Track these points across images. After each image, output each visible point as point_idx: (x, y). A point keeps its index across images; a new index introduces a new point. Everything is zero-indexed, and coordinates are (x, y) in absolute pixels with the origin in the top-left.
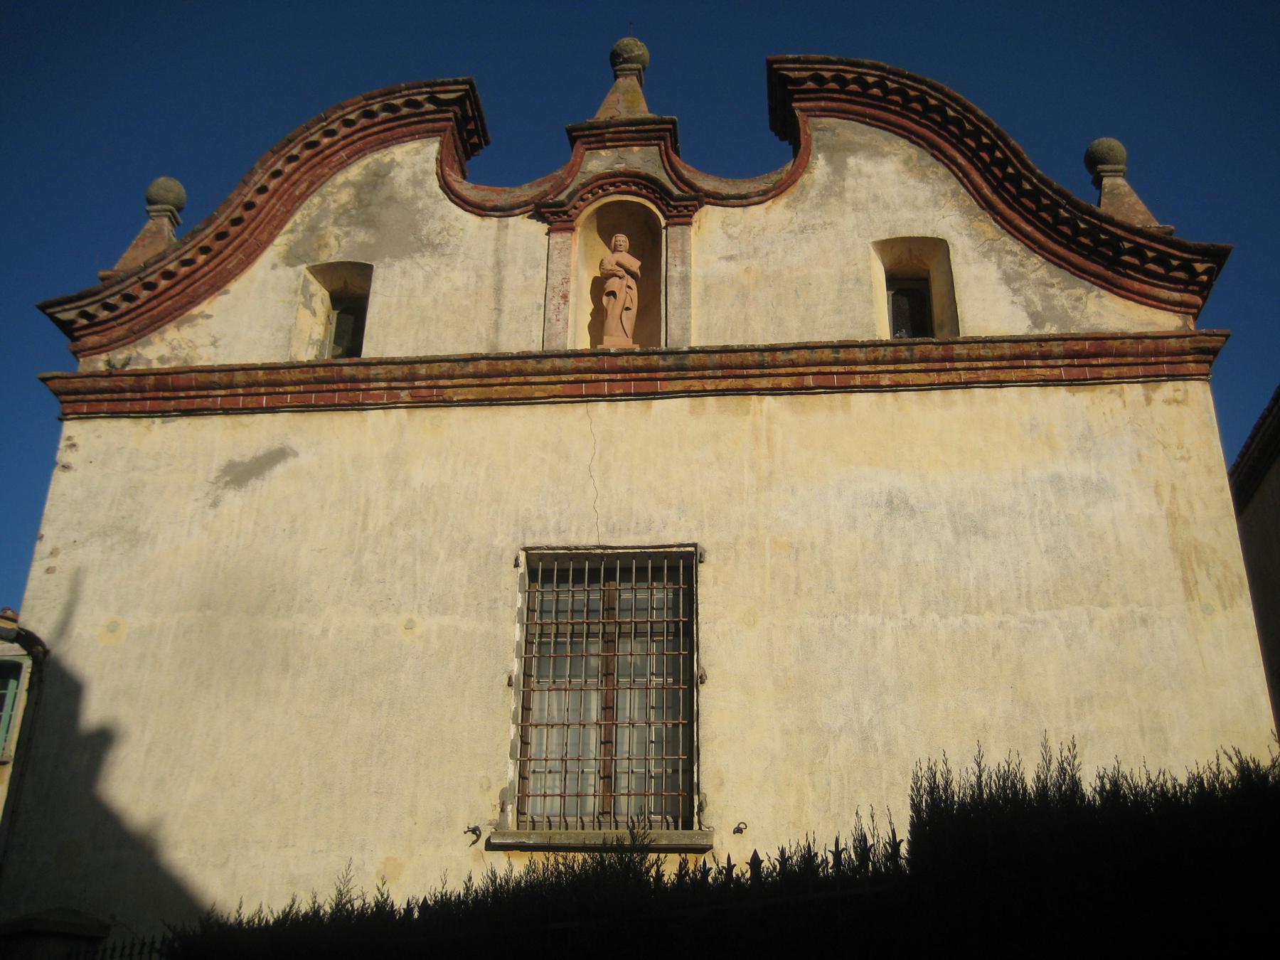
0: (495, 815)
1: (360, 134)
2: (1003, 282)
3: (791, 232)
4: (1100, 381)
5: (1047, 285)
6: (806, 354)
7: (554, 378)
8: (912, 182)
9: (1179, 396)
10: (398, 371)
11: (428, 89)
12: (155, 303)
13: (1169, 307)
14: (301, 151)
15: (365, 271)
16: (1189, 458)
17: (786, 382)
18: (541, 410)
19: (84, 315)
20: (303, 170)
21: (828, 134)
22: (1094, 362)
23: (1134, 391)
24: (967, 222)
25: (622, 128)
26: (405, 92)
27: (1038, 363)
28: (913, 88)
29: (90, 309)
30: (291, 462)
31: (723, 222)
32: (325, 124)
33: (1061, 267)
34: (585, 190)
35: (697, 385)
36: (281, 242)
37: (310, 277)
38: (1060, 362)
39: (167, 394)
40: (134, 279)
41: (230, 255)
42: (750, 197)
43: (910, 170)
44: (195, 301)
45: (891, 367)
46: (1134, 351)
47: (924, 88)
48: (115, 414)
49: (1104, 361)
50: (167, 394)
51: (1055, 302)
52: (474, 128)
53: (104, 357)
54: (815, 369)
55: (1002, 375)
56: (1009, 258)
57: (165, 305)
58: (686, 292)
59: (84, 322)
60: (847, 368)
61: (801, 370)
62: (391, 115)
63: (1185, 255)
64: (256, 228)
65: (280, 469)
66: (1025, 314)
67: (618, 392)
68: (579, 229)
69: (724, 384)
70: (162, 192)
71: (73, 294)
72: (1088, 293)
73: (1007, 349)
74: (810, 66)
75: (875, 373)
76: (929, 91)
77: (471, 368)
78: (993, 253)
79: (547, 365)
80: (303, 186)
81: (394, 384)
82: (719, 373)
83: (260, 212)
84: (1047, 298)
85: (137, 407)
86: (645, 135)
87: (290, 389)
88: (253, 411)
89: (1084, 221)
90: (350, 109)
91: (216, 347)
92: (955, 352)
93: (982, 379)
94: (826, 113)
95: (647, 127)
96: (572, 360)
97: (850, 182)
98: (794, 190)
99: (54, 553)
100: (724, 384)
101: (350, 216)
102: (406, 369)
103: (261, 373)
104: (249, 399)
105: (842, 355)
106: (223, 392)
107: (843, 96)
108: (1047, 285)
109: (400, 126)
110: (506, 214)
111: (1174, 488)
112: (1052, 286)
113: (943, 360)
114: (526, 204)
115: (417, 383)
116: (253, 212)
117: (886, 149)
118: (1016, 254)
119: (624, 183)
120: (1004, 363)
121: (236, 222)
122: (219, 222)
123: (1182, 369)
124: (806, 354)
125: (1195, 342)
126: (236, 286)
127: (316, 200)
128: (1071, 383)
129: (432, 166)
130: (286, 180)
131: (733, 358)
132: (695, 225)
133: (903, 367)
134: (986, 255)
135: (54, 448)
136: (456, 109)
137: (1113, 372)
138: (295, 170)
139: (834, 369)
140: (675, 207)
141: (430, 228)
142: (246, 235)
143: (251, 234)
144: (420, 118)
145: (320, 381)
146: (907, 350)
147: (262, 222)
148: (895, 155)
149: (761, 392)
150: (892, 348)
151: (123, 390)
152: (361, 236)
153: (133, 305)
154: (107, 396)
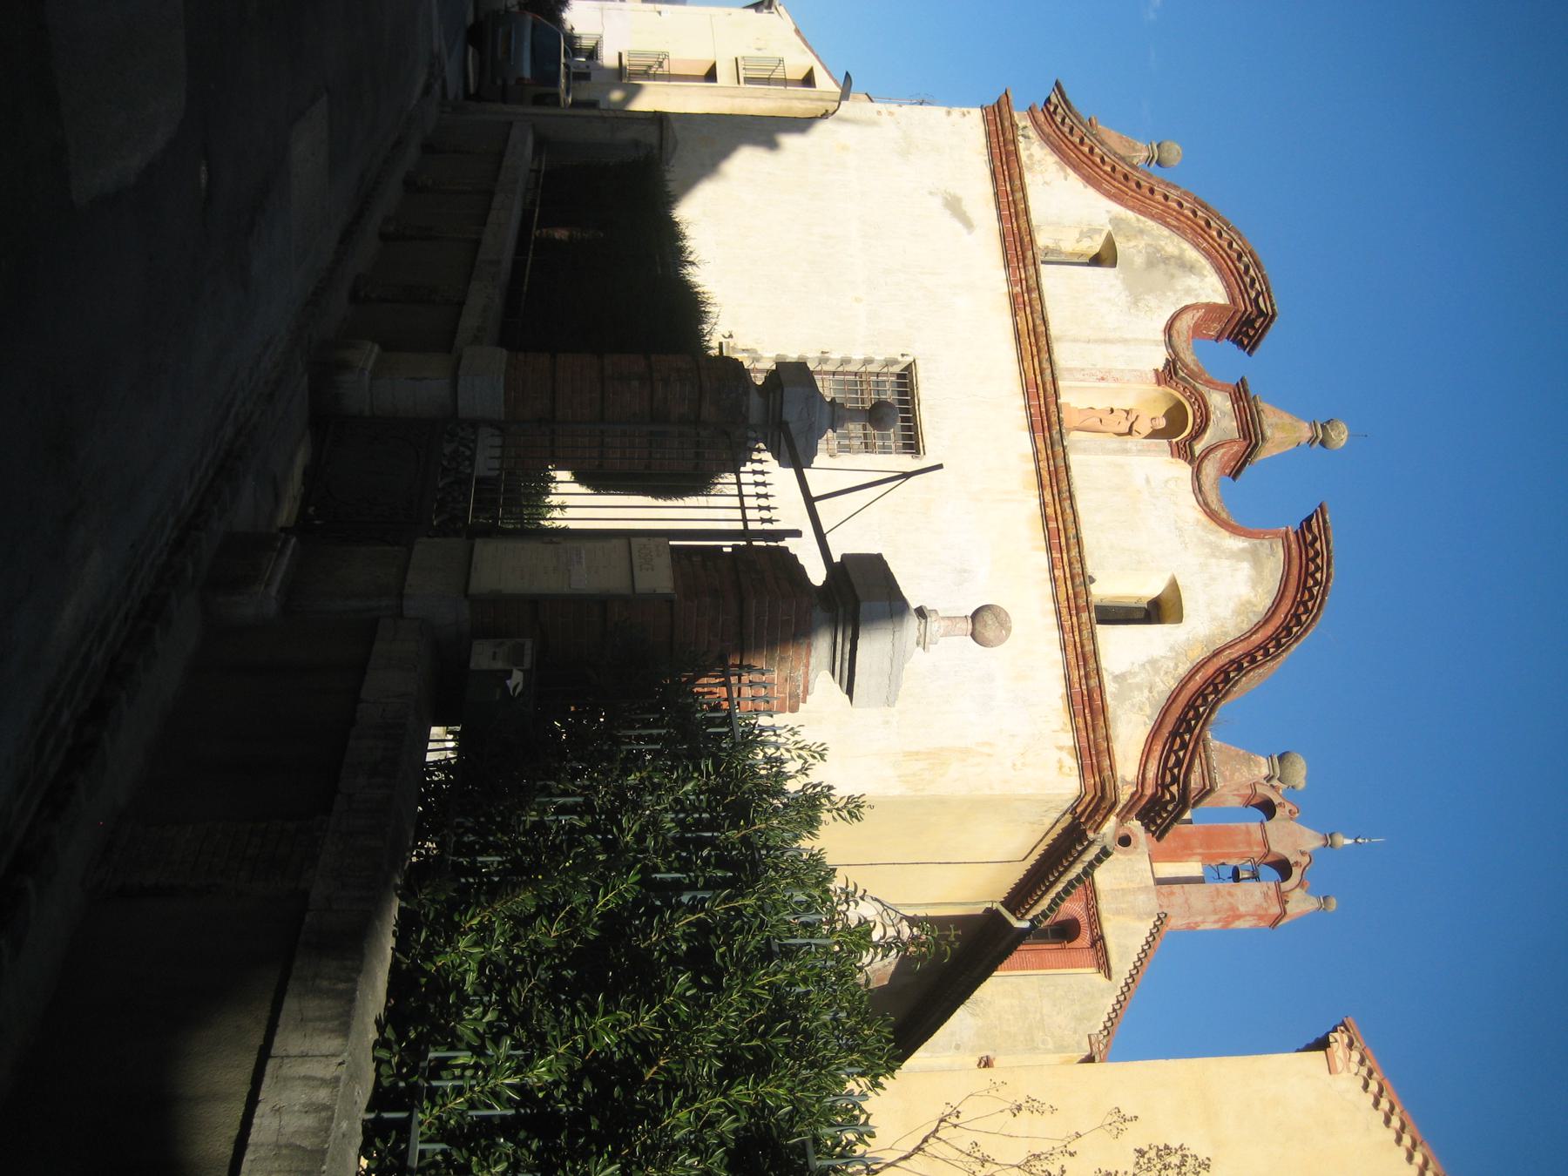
0: (740, 346)
1: (1224, 255)
2: (1150, 658)
3: (1176, 521)
4: (1073, 716)
5: (1151, 688)
6: (1070, 518)
7: (1038, 372)
8: (1232, 605)
9: (1066, 770)
10: (1032, 282)
11: (1264, 290)
12: (1072, 147)
13: (1141, 771)
14: (1201, 218)
15: (1114, 264)
16: (1015, 769)
17: (1050, 511)
18: (1015, 367)
19: (1056, 108)
20: (1189, 222)
21: (1268, 551)
22: (1086, 711)
23: (1068, 739)
24: (1200, 639)
25: (1248, 411)
26: (1260, 276)
27: (1082, 673)
28: (1313, 606)
29: (1060, 110)
30: (965, 231)
31: (1178, 478)
32: (1225, 228)
33: (1168, 700)
34: (1192, 389)
35: (1042, 456)
36: (1130, 215)
37: (1104, 235)
38: (1084, 687)
39: (1004, 159)
40: (1084, 130)
41: (1114, 186)
42: (1201, 495)
43: (1242, 605)
44: (1076, 168)
45: (1068, 575)
46: (1098, 736)
47: (1315, 611)
48: (988, 135)
49: (1089, 718)
50: (1004, 159)
51: (1136, 693)
52: (1251, 334)
53: (1029, 123)
54: (1061, 527)
55: (1070, 648)
56: (1172, 665)
57: (1072, 154)
58: (1115, 452)
59: (1052, 109)
60: (1064, 548)
61: (1060, 519)
62: (1242, 272)
63: (1182, 777)
64: (1137, 199)
65: (958, 226)
66: (1124, 670)
67: (1032, 410)
68: (1160, 388)
69: (1045, 474)
70: (1166, 148)
71: (1067, 97)
72: (1148, 717)
73: (1089, 648)
74: (1322, 532)
75: (1063, 566)
76: (1313, 614)
77: (1038, 322)
78: (1174, 654)
79: (1046, 365)
80: (1175, 223)
81: (1024, 282)
82: (1052, 468)
83: (1149, 199)
84: (1139, 687)
85: (994, 145)
86: (1246, 427)
87: (1015, 225)
88: (998, 208)
89: (1205, 710)
90: (1240, 243)
91: (1043, 185)
92: (1083, 614)
93: (1066, 636)
94: (1286, 550)
95: (1251, 426)
96: (1051, 379)
97: (1227, 563)
98: (1213, 526)
99: (891, 114)
100: (1045, 474)
101: (1155, 254)
102: (1035, 285)
103: (1023, 206)
104: (1006, 204)
105: (1073, 541)
106: (1009, 189)
107: (1304, 562)
108: (1151, 688)
109: (1236, 279)
110: (1168, 345)
111: (989, 755)
112: (1151, 692)
113: (1077, 608)
114: (1176, 354)
115: (1026, 295)
116: (1148, 194)
117: (1260, 590)
118: (1176, 670)
119: (1201, 414)
120: (1079, 650)
121: (1138, 185)
122: (1135, 173)
123: (1088, 774)
124: (1070, 518)
125: (1109, 780)
126: (1091, 192)
127: (1166, 232)
128: (1070, 697)
129: (1204, 300)
130: (1178, 213)
131: (1063, 475)
132: (1173, 460)
133: (1069, 583)
134: (1172, 648)
135: (961, 105)
136: (1255, 312)
137: (1081, 725)
138: (1187, 217)
139: (1063, 540)
140: (1185, 445)
141: (1152, 301)
142: (1130, 193)
143: (1131, 196)
144: (1244, 291)
145: (1021, 240)
146: (1081, 582)
147: (1143, 202)
148: (1256, 596)
149: (1042, 496)
150: (1081, 572)
151: (1003, 135)
152: (1139, 260)
153: (1067, 134)
154: (1000, 127)
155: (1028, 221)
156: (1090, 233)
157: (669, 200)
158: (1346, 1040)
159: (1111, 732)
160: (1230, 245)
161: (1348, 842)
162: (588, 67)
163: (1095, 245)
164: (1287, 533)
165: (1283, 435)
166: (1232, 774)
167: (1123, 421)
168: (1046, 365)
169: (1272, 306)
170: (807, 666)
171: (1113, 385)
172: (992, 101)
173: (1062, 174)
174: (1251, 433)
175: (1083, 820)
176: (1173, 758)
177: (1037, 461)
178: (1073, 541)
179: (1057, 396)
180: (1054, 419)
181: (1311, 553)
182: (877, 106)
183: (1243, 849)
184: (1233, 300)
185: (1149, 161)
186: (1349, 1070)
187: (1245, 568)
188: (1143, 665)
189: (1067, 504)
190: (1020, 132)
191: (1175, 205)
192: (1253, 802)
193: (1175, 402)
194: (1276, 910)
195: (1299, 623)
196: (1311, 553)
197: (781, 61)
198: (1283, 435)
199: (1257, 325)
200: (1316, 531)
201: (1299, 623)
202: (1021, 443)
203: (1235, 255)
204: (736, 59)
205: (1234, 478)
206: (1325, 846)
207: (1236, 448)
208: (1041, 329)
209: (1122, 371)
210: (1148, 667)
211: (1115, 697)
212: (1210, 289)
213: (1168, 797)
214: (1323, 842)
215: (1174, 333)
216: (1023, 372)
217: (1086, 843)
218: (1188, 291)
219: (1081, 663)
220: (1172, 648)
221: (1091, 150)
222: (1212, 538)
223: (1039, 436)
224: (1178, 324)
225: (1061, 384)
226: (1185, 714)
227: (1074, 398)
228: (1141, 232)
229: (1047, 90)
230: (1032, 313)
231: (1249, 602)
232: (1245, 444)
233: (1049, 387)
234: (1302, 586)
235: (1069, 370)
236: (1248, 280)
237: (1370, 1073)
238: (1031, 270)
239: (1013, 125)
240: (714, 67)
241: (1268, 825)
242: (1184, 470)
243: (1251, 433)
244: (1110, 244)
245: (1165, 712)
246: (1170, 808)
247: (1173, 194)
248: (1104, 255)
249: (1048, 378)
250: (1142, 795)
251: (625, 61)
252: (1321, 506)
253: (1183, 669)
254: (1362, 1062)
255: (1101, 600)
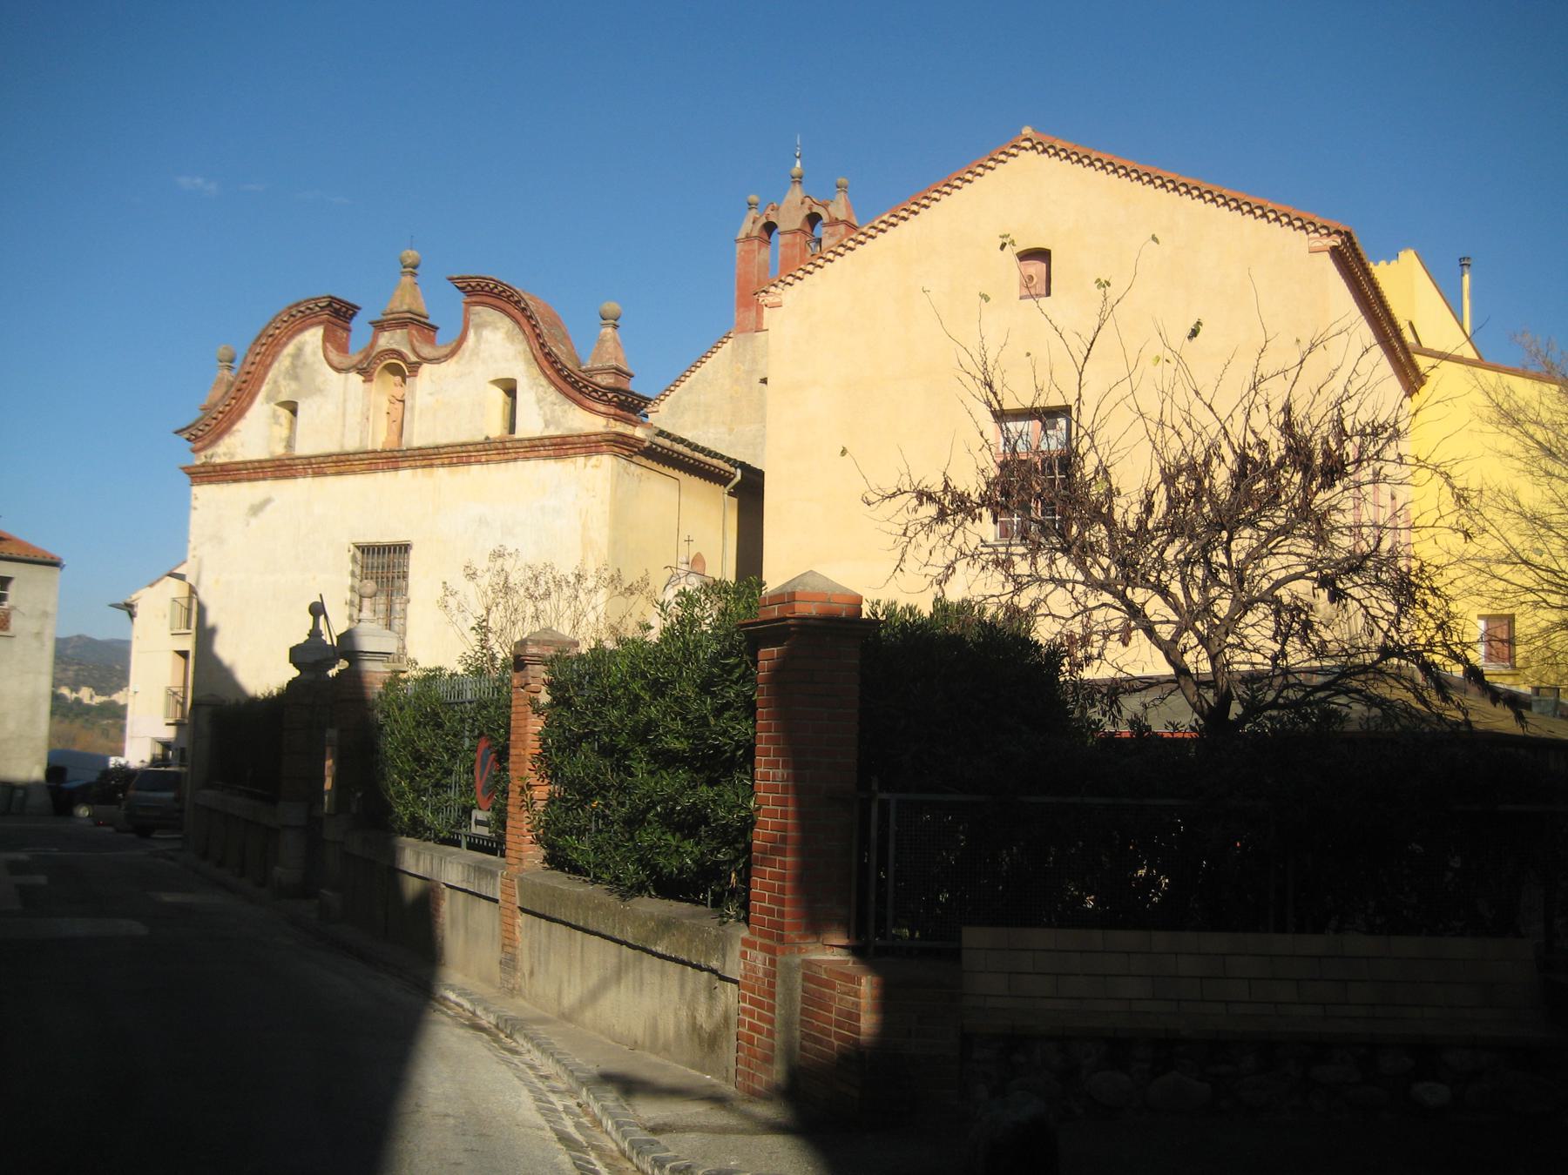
4: (567, 456)
7: (362, 462)
8: (508, 345)
9: (598, 463)
10: (305, 461)
15: (296, 403)
17: (446, 461)
21: (477, 316)
23: (581, 460)
27: (542, 448)
35: (413, 463)
36: (264, 389)
37: (277, 407)
38: (550, 448)
44: (233, 423)
45: (484, 453)
48: (210, 482)
49: (568, 446)
54: (456, 455)
55: (528, 455)
56: (541, 389)
59: (193, 437)
65: (269, 508)
68: (375, 380)
77: (330, 459)
79: (357, 457)
82: (421, 458)
84: (553, 411)
87: (269, 470)
98: (460, 352)
99: (195, 549)
105: (464, 449)
112: (555, 404)
113: (504, 449)
116: (250, 375)
120: (528, 449)
121: (244, 382)
123: (600, 449)
128: (557, 457)
129: (320, 343)
131: (424, 452)
132: (419, 375)
134: (531, 388)
136: (329, 308)
138: (267, 349)
139: (464, 454)
145: (279, 466)
149: (438, 466)
152: (294, 386)
155: (267, 461)
156: (275, 417)
157: (254, 702)
158: (764, 294)
159: (575, 433)
160: (285, 321)
161: (798, 164)
162: (176, 749)
163: (284, 413)
164: (466, 303)
165: (407, 297)
166: (609, 353)
167: (396, 406)
168: (357, 457)
169: (324, 298)
170: (376, 672)
171: (372, 410)
172: (187, 479)
173: (237, 434)
174: (401, 322)
175: (636, 450)
176: (594, 394)
177: (416, 467)
178: (464, 449)
179: (375, 452)
180: (390, 454)
181: (478, 288)
182: (189, 557)
183: (797, 251)
184: (320, 323)
185: (230, 368)
186: (780, 294)
187: (487, 333)
188: (541, 408)
189: (442, 451)
190: (208, 460)
191: (258, 358)
192: (767, 238)
193: (386, 372)
194: (842, 228)
195: (519, 302)
196: (478, 288)
197: (174, 600)
198: (407, 297)
199: (338, 306)
200: (465, 284)
201: (519, 302)
202: (406, 477)
203: (292, 319)
204: (173, 634)
205: (437, 328)
206: (800, 182)
207: (414, 332)
208: (334, 458)
209: (363, 406)
210: (541, 405)
211: (558, 428)
212: (313, 337)
213: (615, 399)
214: (797, 185)
215: (339, 367)
216: (362, 472)
217: (654, 446)
218: (314, 353)
219: (536, 449)
220: (531, 388)
221: (220, 412)
222: (467, 354)
223: (401, 464)
224: (336, 363)
225: (370, 448)
226: (569, 383)
227: (379, 438)
228: (275, 382)
229: (181, 439)
230: (325, 463)
231: (507, 333)
232: (410, 325)
233: (370, 456)
234: (499, 296)
235: (361, 440)
236: (308, 312)
237: (781, 281)
238: (297, 462)
239: (203, 465)
240: (179, 653)
241: (781, 228)
242: (426, 369)
243: (401, 322)
244: (284, 404)
245: (567, 396)
246: (623, 398)
247: (250, 359)
248: (291, 408)
249: (365, 456)
250: (615, 415)
251: (171, 722)
252: (450, 279)
253: (544, 381)
254: (776, 286)
255: (505, 428)
